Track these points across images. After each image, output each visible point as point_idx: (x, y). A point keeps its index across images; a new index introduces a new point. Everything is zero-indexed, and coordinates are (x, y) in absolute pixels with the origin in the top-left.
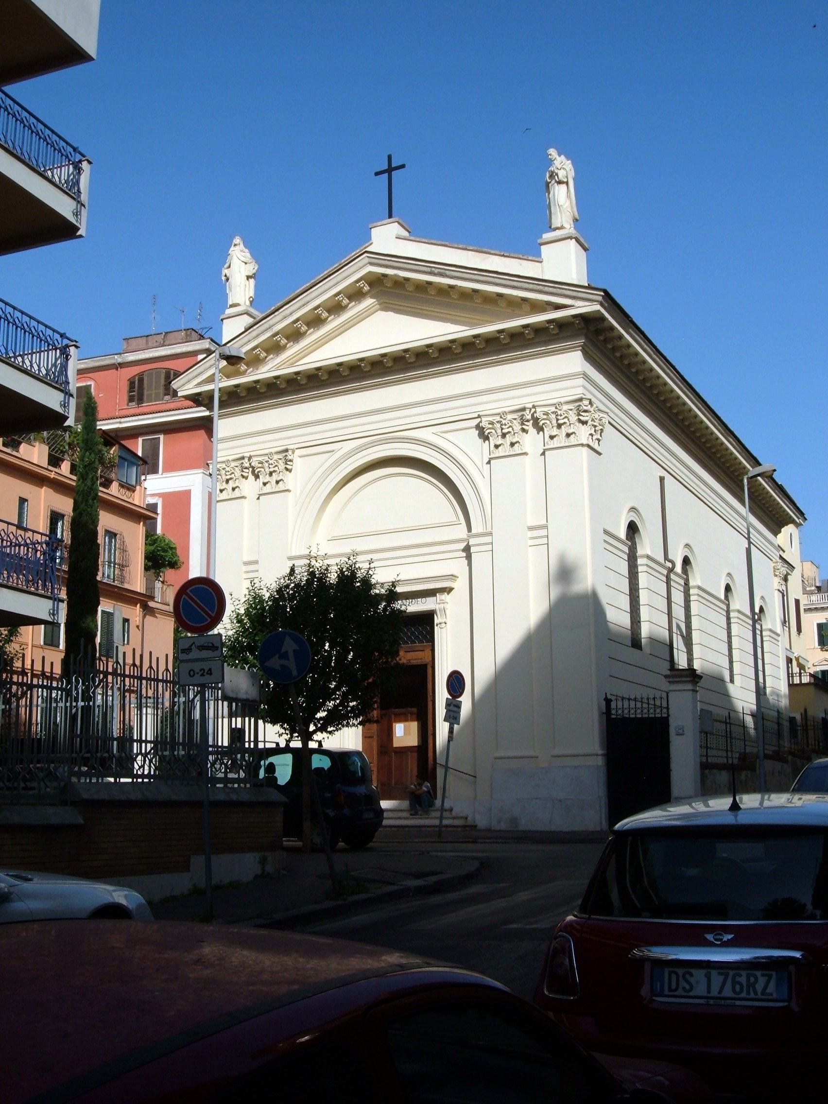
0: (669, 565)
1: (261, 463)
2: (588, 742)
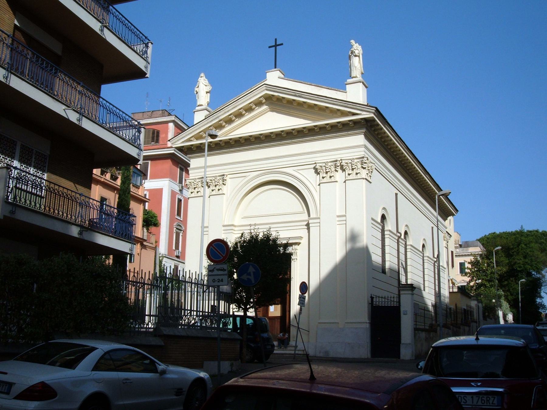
0: (399, 235)
1: (211, 180)
2: (363, 317)
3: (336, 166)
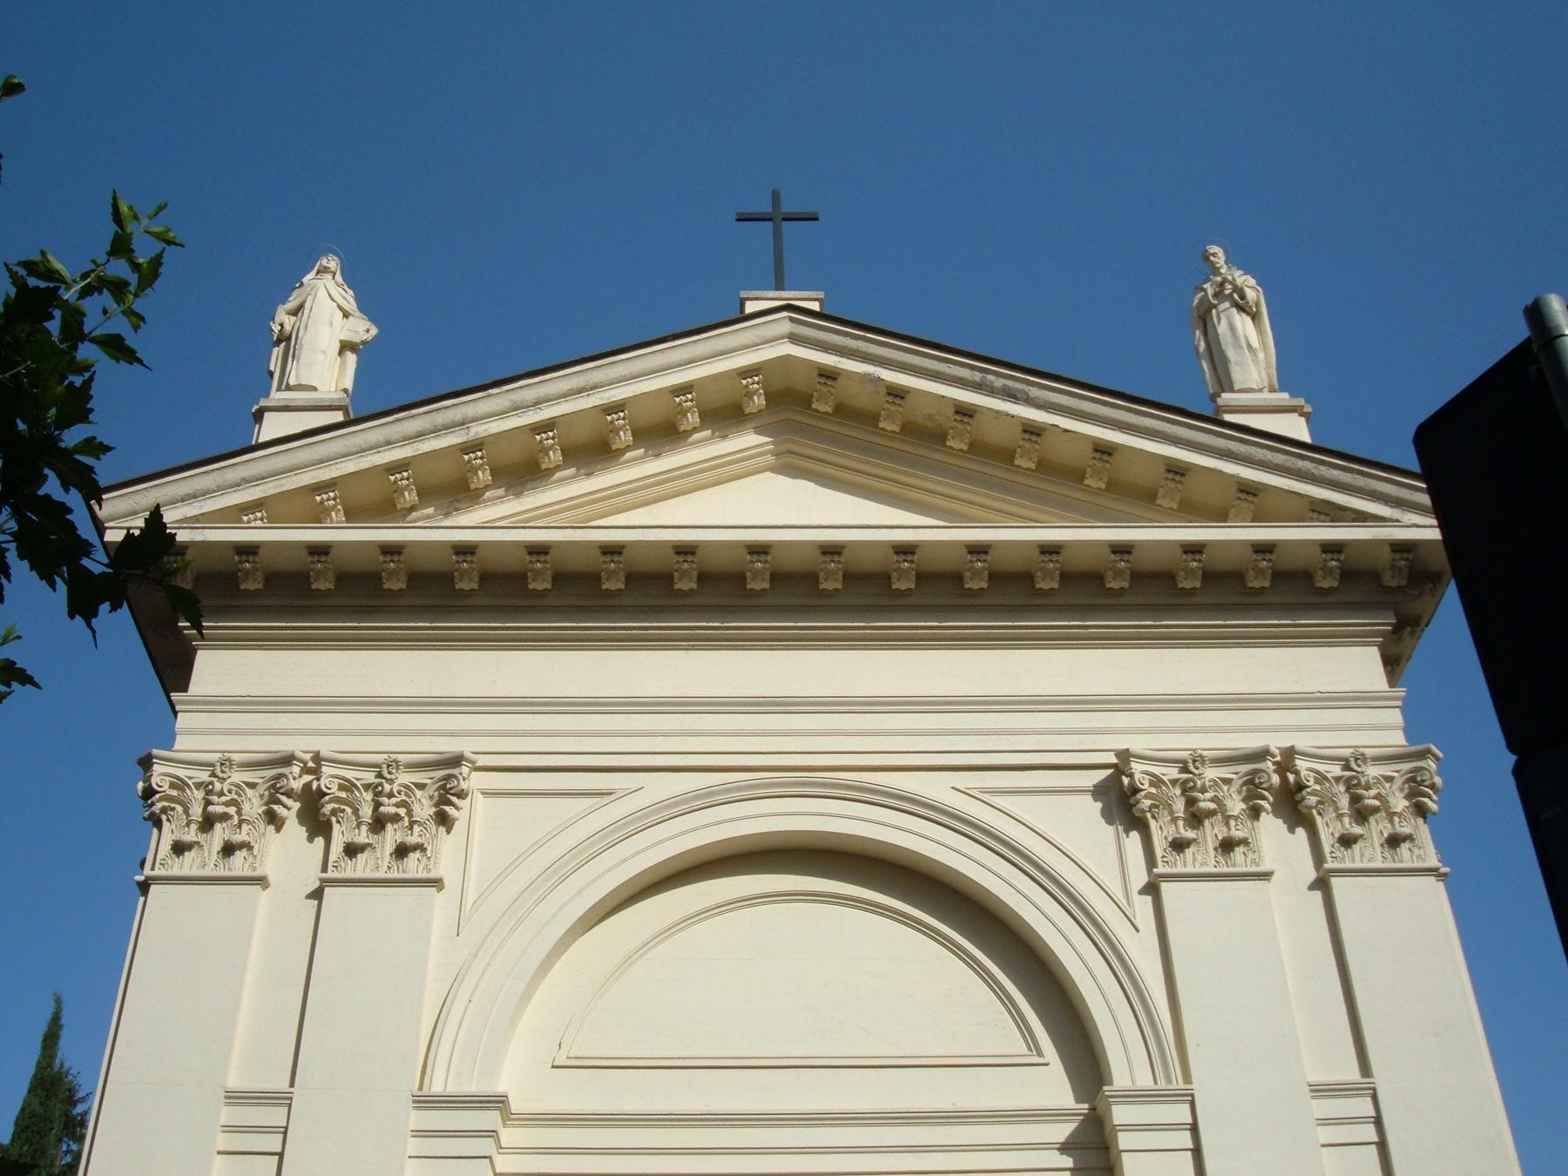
3: (275, 793)
